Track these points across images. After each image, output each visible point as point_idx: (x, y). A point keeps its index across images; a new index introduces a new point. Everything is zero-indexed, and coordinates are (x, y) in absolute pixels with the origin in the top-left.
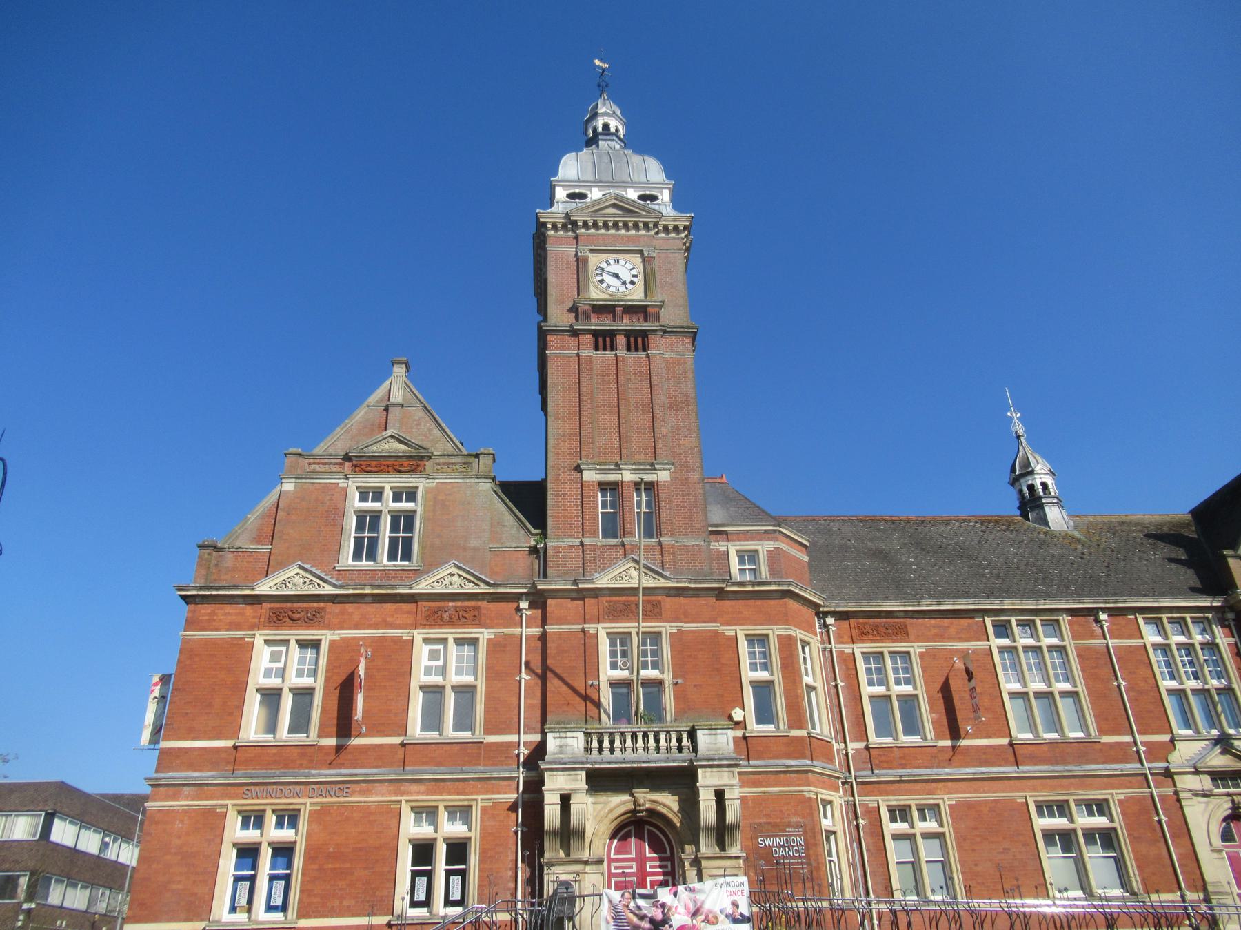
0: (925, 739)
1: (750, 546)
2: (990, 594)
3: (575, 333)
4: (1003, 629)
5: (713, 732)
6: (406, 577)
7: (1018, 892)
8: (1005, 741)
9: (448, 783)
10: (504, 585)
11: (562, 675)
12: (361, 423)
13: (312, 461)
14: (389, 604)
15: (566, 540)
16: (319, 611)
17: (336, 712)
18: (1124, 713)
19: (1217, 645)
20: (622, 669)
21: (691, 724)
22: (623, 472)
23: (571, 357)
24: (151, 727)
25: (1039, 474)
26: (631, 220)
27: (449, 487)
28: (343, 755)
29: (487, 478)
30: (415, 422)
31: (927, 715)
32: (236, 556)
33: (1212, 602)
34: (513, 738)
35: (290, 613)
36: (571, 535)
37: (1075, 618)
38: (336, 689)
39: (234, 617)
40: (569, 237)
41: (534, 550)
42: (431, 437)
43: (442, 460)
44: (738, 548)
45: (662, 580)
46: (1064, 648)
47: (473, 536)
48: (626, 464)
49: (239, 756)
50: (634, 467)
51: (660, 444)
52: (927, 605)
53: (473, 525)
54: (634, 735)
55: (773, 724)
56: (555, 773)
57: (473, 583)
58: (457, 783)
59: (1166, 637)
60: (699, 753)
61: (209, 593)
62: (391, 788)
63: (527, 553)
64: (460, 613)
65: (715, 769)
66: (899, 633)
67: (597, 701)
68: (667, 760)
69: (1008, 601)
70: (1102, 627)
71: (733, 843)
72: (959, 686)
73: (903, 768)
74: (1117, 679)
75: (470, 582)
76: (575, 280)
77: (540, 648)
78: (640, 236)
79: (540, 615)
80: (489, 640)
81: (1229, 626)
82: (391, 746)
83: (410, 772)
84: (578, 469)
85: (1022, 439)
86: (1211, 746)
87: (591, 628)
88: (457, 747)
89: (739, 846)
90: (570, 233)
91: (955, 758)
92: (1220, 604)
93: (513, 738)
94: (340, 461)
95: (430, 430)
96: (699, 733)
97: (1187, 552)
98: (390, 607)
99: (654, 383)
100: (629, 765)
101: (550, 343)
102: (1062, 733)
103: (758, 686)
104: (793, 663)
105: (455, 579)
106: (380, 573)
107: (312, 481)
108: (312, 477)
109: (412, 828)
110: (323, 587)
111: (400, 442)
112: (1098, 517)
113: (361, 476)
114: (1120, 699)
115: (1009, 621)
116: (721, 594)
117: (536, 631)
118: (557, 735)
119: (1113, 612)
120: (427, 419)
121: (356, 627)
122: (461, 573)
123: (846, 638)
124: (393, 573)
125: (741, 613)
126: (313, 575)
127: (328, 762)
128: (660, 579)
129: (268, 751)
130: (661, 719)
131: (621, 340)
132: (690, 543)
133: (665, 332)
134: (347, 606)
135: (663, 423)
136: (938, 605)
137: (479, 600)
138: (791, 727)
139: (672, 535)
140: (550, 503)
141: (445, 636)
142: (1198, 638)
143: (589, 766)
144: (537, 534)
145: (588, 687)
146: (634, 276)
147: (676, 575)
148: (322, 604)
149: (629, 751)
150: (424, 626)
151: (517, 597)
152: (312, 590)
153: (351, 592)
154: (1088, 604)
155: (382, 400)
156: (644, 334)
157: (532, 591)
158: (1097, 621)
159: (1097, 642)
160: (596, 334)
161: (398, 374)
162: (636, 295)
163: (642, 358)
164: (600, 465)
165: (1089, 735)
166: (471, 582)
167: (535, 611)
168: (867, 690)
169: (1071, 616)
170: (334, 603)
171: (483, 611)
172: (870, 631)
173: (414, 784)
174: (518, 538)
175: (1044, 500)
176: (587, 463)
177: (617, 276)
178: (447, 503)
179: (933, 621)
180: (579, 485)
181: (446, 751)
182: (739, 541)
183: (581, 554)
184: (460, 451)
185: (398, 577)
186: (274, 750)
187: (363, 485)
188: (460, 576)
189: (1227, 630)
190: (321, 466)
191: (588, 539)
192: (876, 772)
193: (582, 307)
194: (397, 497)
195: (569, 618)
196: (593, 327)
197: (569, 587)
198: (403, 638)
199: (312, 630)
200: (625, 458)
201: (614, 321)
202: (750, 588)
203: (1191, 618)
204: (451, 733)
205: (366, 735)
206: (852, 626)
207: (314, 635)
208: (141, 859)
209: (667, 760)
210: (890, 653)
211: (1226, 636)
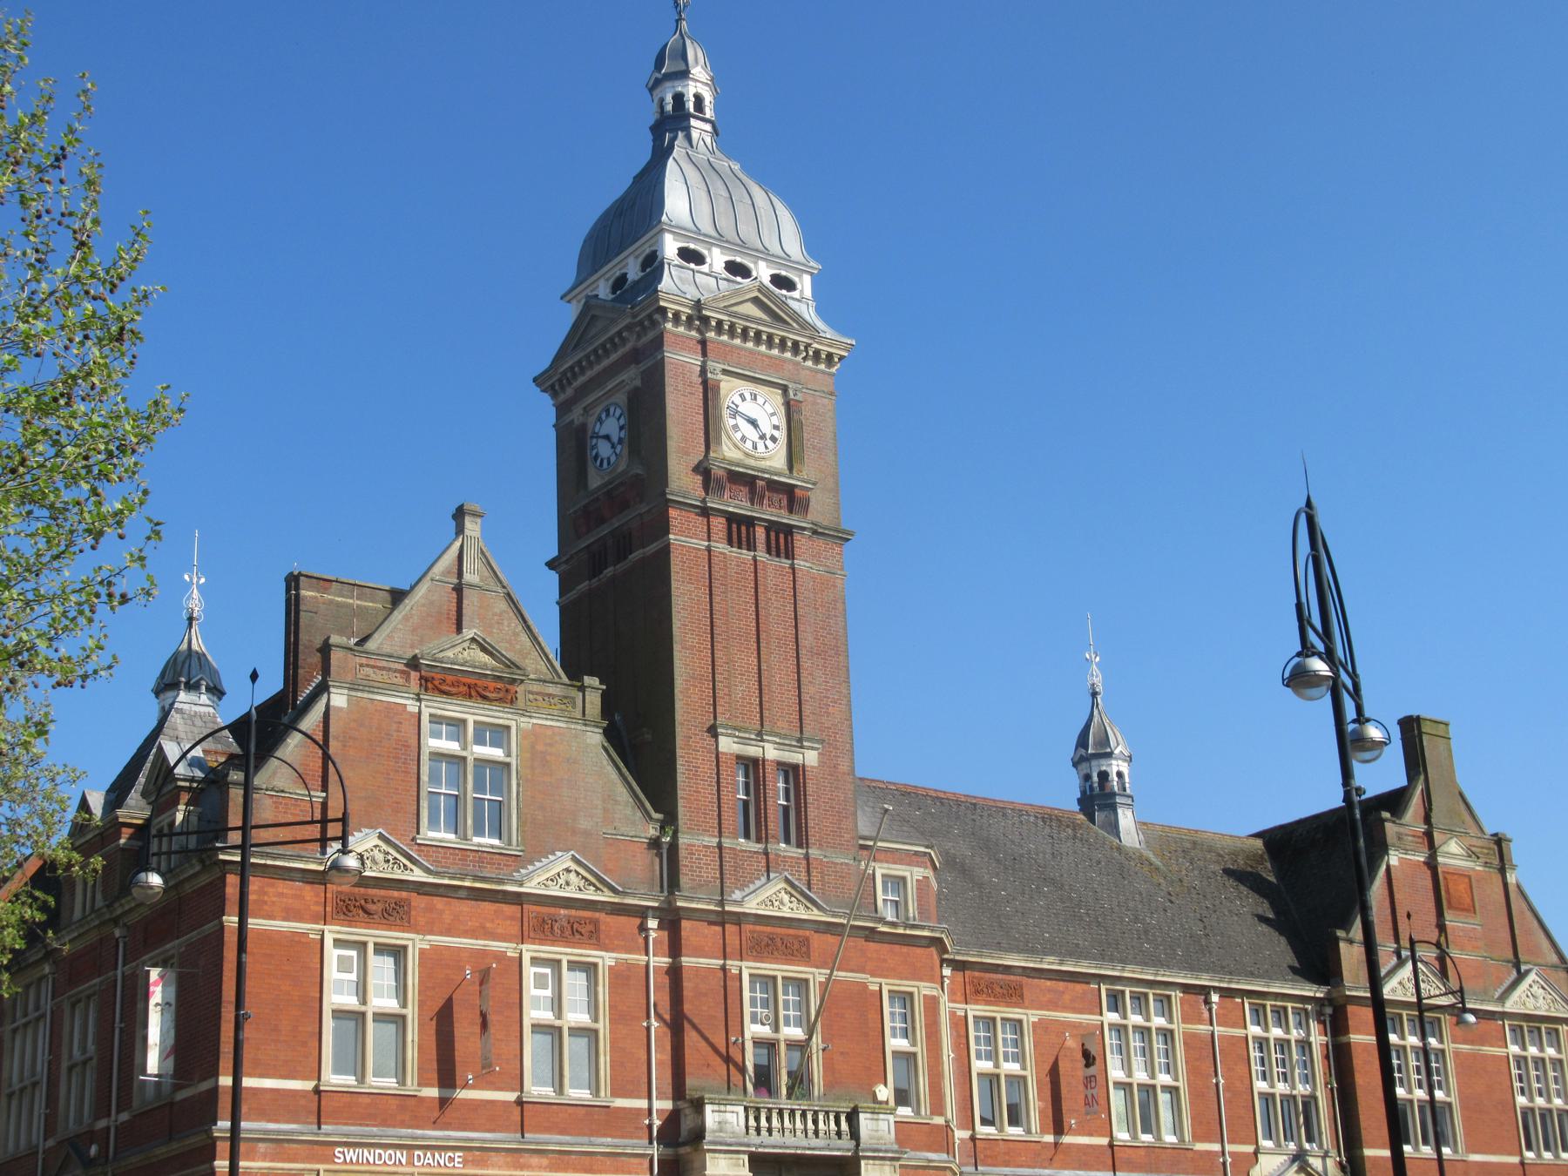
0: (1029, 1132)
1: (899, 870)
2: (1103, 957)
3: (705, 512)
4: (1116, 1002)
5: (875, 1116)
6: (505, 865)
8: (1104, 1141)
9: (573, 1157)
10: (633, 895)
11: (699, 1027)
12: (423, 605)
13: (364, 661)
14: (487, 903)
15: (701, 838)
16: (399, 904)
17: (434, 1052)
18: (1217, 1117)
19: (1310, 1044)
20: (763, 1024)
21: (852, 1106)
22: (767, 745)
23: (699, 550)
24: (158, 1048)
25: (1116, 759)
27: (549, 732)
28: (450, 1112)
29: (597, 727)
30: (496, 618)
31: (1035, 1105)
32: (276, 802)
33: (1316, 992)
35: (363, 902)
36: (705, 831)
37: (1187, 996)
38: (432, 1019)
39: (290, 901)
40: (691, 339)
41: (655, 844)
42: (518, 647)
43: (536, 687)
45: (816, 911)
46: (1172, 1032)
47: (582, 813)
48: (771, 735)
50: (778, 740)
51: (807, 709)
52: (1050, 963)
53: (582, 796)
55: (1152, 1133)
56: (717, 1155)
57: (594, 886)
58: (583, 1157)
59: (1266, 1029)
60: (862, 1141)
61: (263, 862)
62: (509, 1159)
63: (645, 846)
64: (575, 926)
65: (877, 1162)
66: (1013, 995)
67: (741, 1064)
68: (828, 1148)
69: (1129, 967)
70: (1210, 1010)
72: (1072, 1071)
73: (1006, 1166)
74: (1216, 1075)
75: (589, 885)
76: (701, 418)
77: (668, 985)
78: (785, 360)
79: (667, 939)
80: (610, 967)
81: (1323, 1023)
82: (504, 1102)
84: (713, 731)
85: (1099, 697)
86: (1288, 1162)
87: (733, 965)
88: (583, 1110)
90: (694, 333)
91: (1056, 1158)
92: (1322, 995)
94: (401, 667)
95: (516, 634)
96: (862, 1116)
97: (1273, 905)
98: (487, 907)
99: (800, 612)
100: (793, 1151)
101: (673, 522)
102: (1159, 1138)
103: (908, 1058)
104: (937, 1032)
105: (572, 876)
106: (472, 854)
107: (371, 696)
108: (372, 689)
110: (411, 870)
111: (484, 649)
112: (1167, 829)
113: (438, 699)
114: (1215, 1099)
115: (1123, 992)
116: (871, 934)
117: (664, 961)
118: (716, 1107)
119: (1227, 993)
120: (512, 614)
121: (448, 932)
123: (960, 996)
124: (489, 856)
125: (885, 961)
126: (398, 852)
127: (433, 1120)
128: (814, 909)
129: (360, 1100)
130: (808, 1095)
131: (760, 533)
132: (838, 861)
133: (815, 532)
134: (436, 900)
135: (810, 678)
136: (1060, 964)
137: (596, 910)
138: (933, 1113)
139: (820, 847)
140: (680, 778)
141: (558, 957)
142: (1295, 1034)
143: (754, 1149)
144: (657, 820)
145: (730, 1045)
146: (744, 399)
148: (404, 894)
150: (533, 941)
151: (642, 913)
152: (398, 875)
153: (446, 882)
154: (1204, 981)
155: (449, 572)
156: (788, 530)
157: (665, 906)
158: (1207, 1002)
159: (1203, 1028)
160: (731, 518)
161: (473, 534)
162: (773, 458)
163: (785, 568)
164: (739, 731)
165: (1182, 1140)
166: (591, 884)
167: (661, 933)
168: (981, 1066)
169: (1183, 992)
170: (419, 894)
171: (603, 927)
172: (985, 990)
173: (535, 1155)
174: (634, 823)
175: (1118, 800)
176: (726, 727)
177: (753, 423)
178: (548, 758)
179: (1049, 983)
180: (714, 756)
181: (570, 1114)
182: (887, 862)
183: (717, 859)
184: (560, 677)
185: (494, 864)
186: (367, 1100)
187: (440, 712)
188: (578, 874)
189: (1321, 1026)
190: (377, 671)
191: (728, 841)
193: (717, 472)
195: (707, 949)
196: (731, 509)
197: (712, 907)
198: (508, 954)
199: (395, 931)
200: (767, 728)
201: (752, 504)
202: (900, 931)
203: (1292, 1008)
204: (578, 1094)
205: (473, 1087)
206: (967, 980)
207: (397, 938)
209: (828, 1148)
210: (1002, 1019)
211: (1320, 1034)
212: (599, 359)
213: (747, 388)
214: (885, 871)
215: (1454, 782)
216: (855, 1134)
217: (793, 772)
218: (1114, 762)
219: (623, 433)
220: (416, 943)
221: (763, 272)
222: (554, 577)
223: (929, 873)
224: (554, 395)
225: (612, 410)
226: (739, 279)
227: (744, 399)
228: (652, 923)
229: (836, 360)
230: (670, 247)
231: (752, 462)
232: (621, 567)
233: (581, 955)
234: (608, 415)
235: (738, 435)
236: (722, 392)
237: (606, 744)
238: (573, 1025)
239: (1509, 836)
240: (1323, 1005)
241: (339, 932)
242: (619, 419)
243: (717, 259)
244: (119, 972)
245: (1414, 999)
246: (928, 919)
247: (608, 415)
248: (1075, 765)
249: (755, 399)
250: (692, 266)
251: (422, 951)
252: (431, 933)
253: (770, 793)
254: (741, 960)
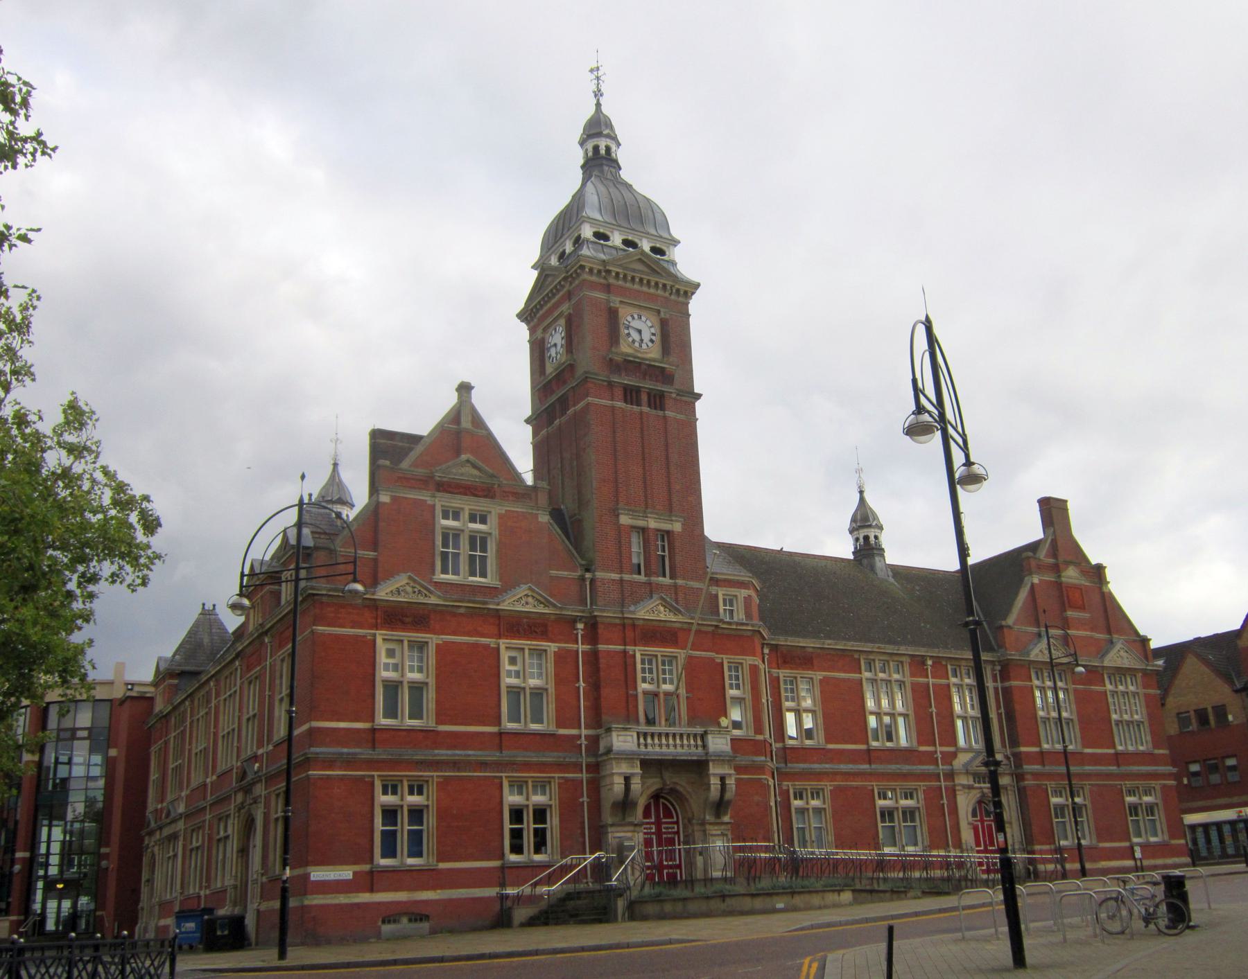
7: (770, 859)
22: (649, 520)
26: (653, 279)
34: (574, 732)
44: (443, 503)
45: (680, 617)
49: (373, 736)
52: (828, 645)
54: (674, 735)
71: (725, 813)
80: (555, 652)
83: (507, 755)
89: (729, 816)
93: (574, 732)
105: (530, 600)
109: (512, 798)
121: (454, 633)
122: (535, 595)
123: (774, 665)
131: (644, 398)
146: (633, 318)
147: (327, 514)
149: (686, 748)
156: (662, 395)
162: (651, 352)
166: (541, 603)
177: (640, 332)
182: (725, 587)
192: (789, 765)
194: (473, 519)
208: (1182, 819)
212: (550, 299)
213: (635, 312)
214: (724, 592)
216: (704, 746)
217: (666, 535)
218: (873, 530)
220: (434, 640)
222: (529, 429)
223: (752, 592)
227: (633, 318)
228: (580, 626)
231: (639, 355)
232: (564, 419)
233: (537, 645)
235: (630, 339)
236: (620, 314)
237: (551, 521)
238: (532, 686)
239: (1104, 565)
240: (995, 665)
241: (385, 635)
243: (617, 239)
244: (268, 663)
245: (1049, 660)
246: (751, 619)
248: (851, 532)
250: (602, 242)
251: (438, 646)
252: (443, 634)
253: (652, 548)
254: (635, 646)
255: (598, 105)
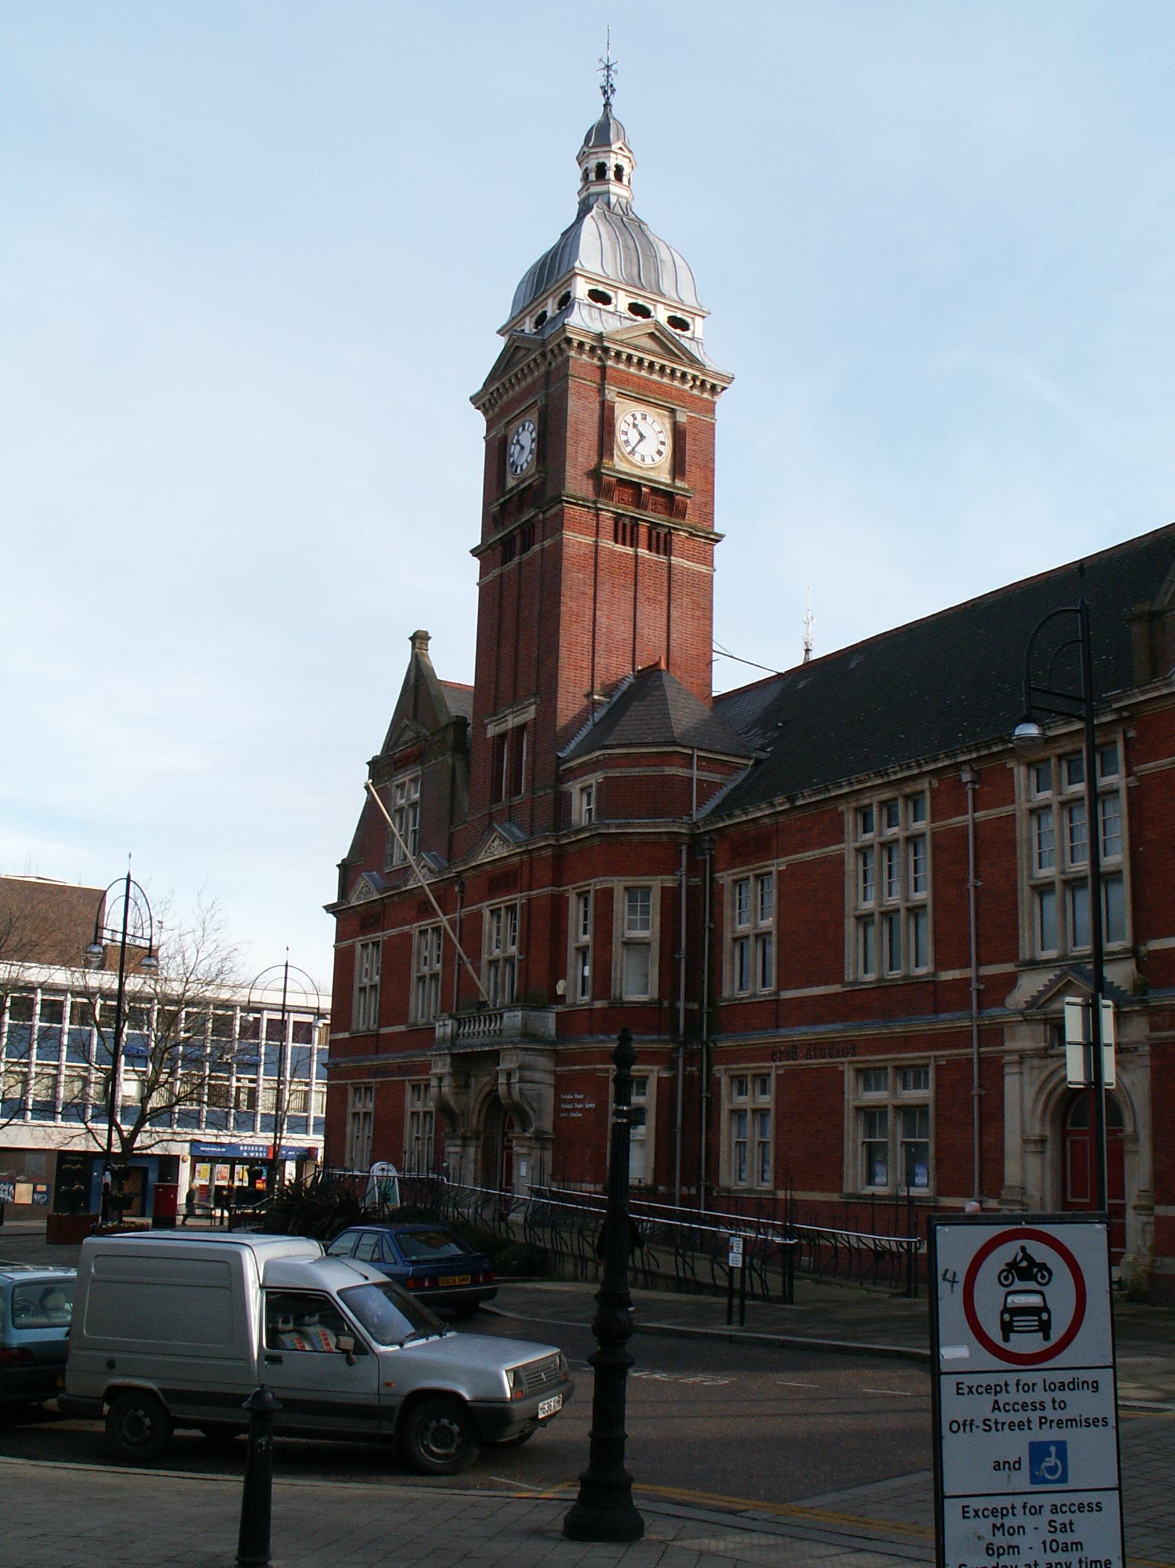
215: (482, 390)
219: (534, 445)
221: (661, 315)
224: (485, 413)
225: (527, 424)
226: (639, 318)
229: (719, 390)
230: (581, 289)
234: (524, 429)
242: (531, 433)
243: (622, 301)
247: (524, 429)
249: (645, 419)
250: (600, 305)
255: (607, 105)
